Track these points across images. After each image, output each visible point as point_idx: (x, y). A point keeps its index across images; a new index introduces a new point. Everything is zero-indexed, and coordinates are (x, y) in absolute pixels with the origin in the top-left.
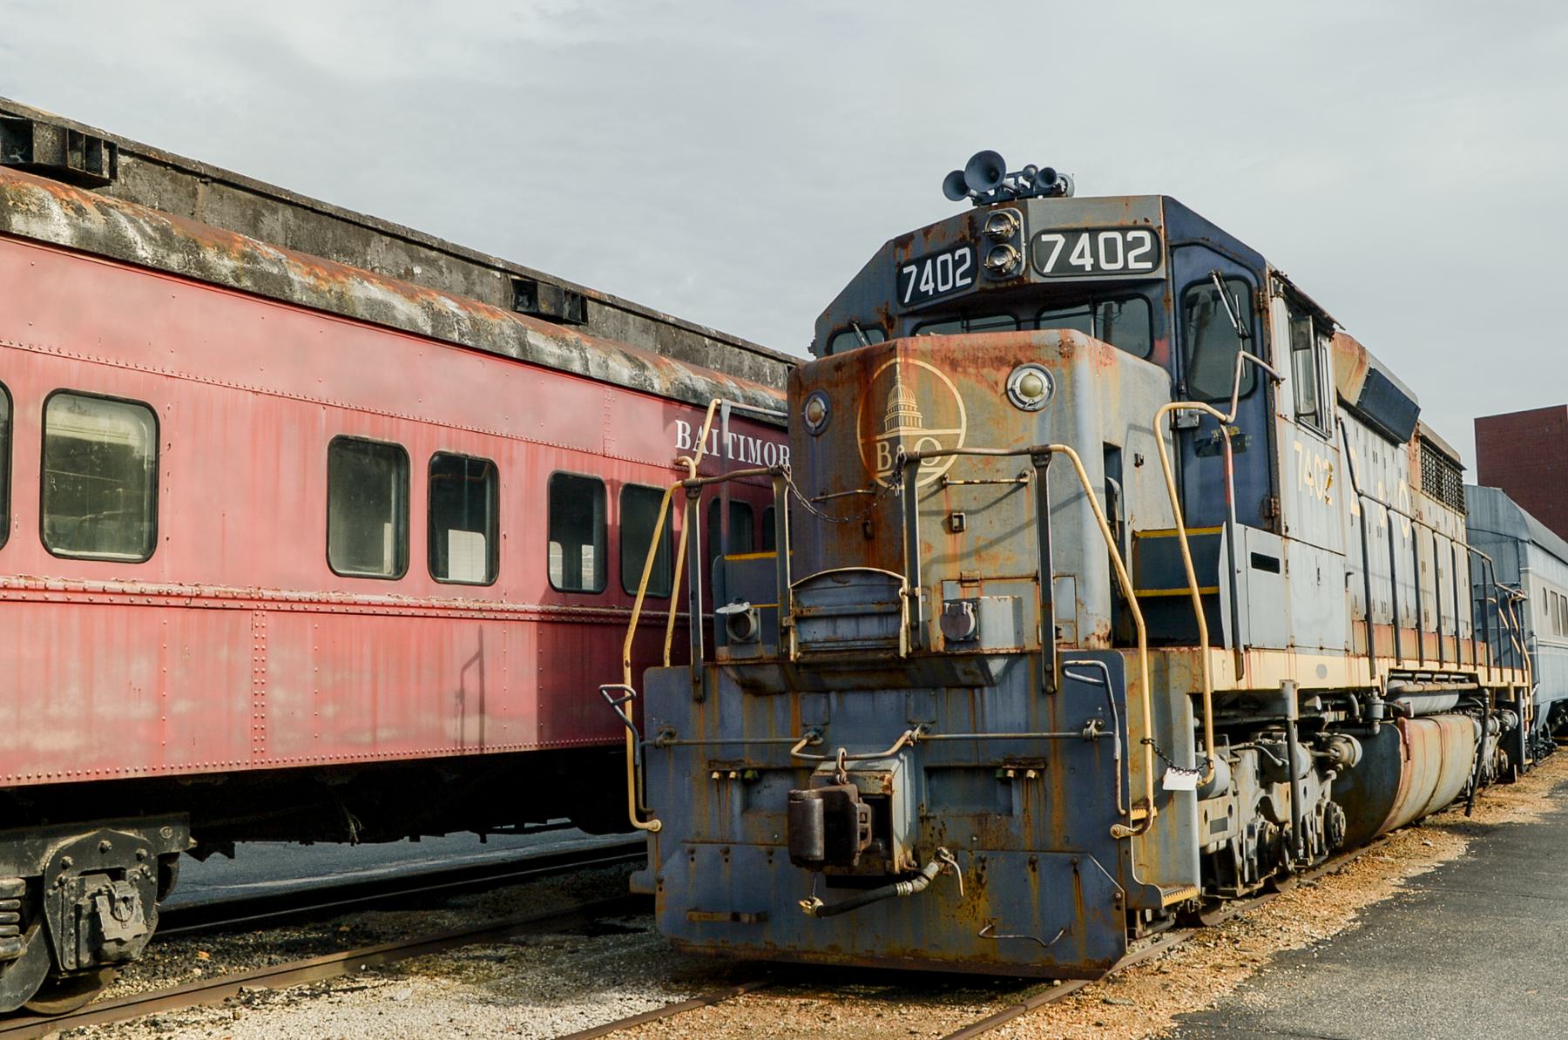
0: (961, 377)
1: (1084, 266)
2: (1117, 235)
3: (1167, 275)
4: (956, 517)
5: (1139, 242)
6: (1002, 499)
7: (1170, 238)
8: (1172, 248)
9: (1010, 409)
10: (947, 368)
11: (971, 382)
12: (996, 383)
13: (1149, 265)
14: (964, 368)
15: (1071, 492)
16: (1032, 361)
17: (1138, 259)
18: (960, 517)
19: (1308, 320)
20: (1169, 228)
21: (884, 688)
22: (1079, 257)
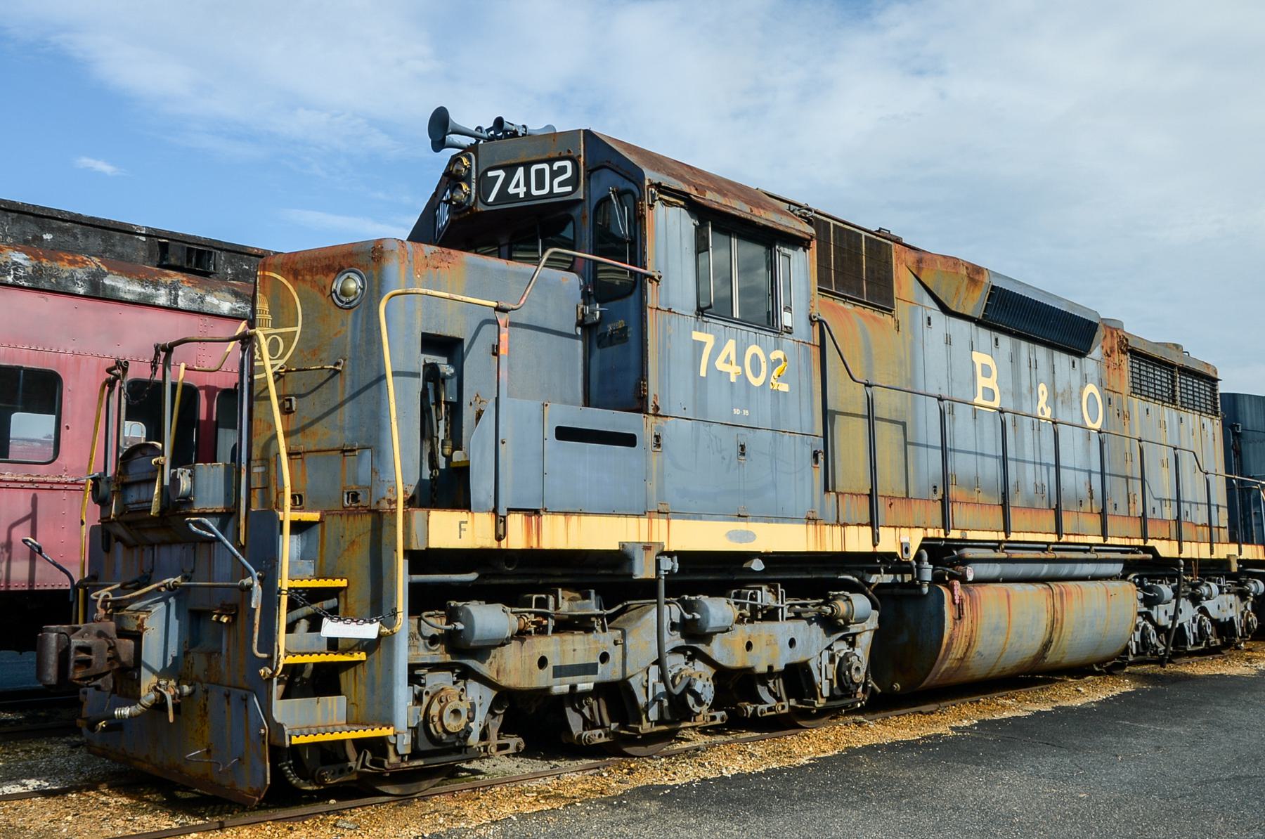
0: (301, 284)
1: (519, 194)
2: (546, 166)
3: (584, 196)
4: (287, 400)
5: (563, 170)
6: (321, 385)
7: (587, 165)
8: (590, 173)
9: (333, 308)
10: (291, 277)
11: (307, 287)
12: (325, 287)
13: (569, 189)
14: (303, 276)
15: (373, 376)
16: (352, 266)
17: (561, 184)
18: (290, 400)
19: (708, 225)
20: (587, 157)
21: (163, 543)
22: (515, 188)
